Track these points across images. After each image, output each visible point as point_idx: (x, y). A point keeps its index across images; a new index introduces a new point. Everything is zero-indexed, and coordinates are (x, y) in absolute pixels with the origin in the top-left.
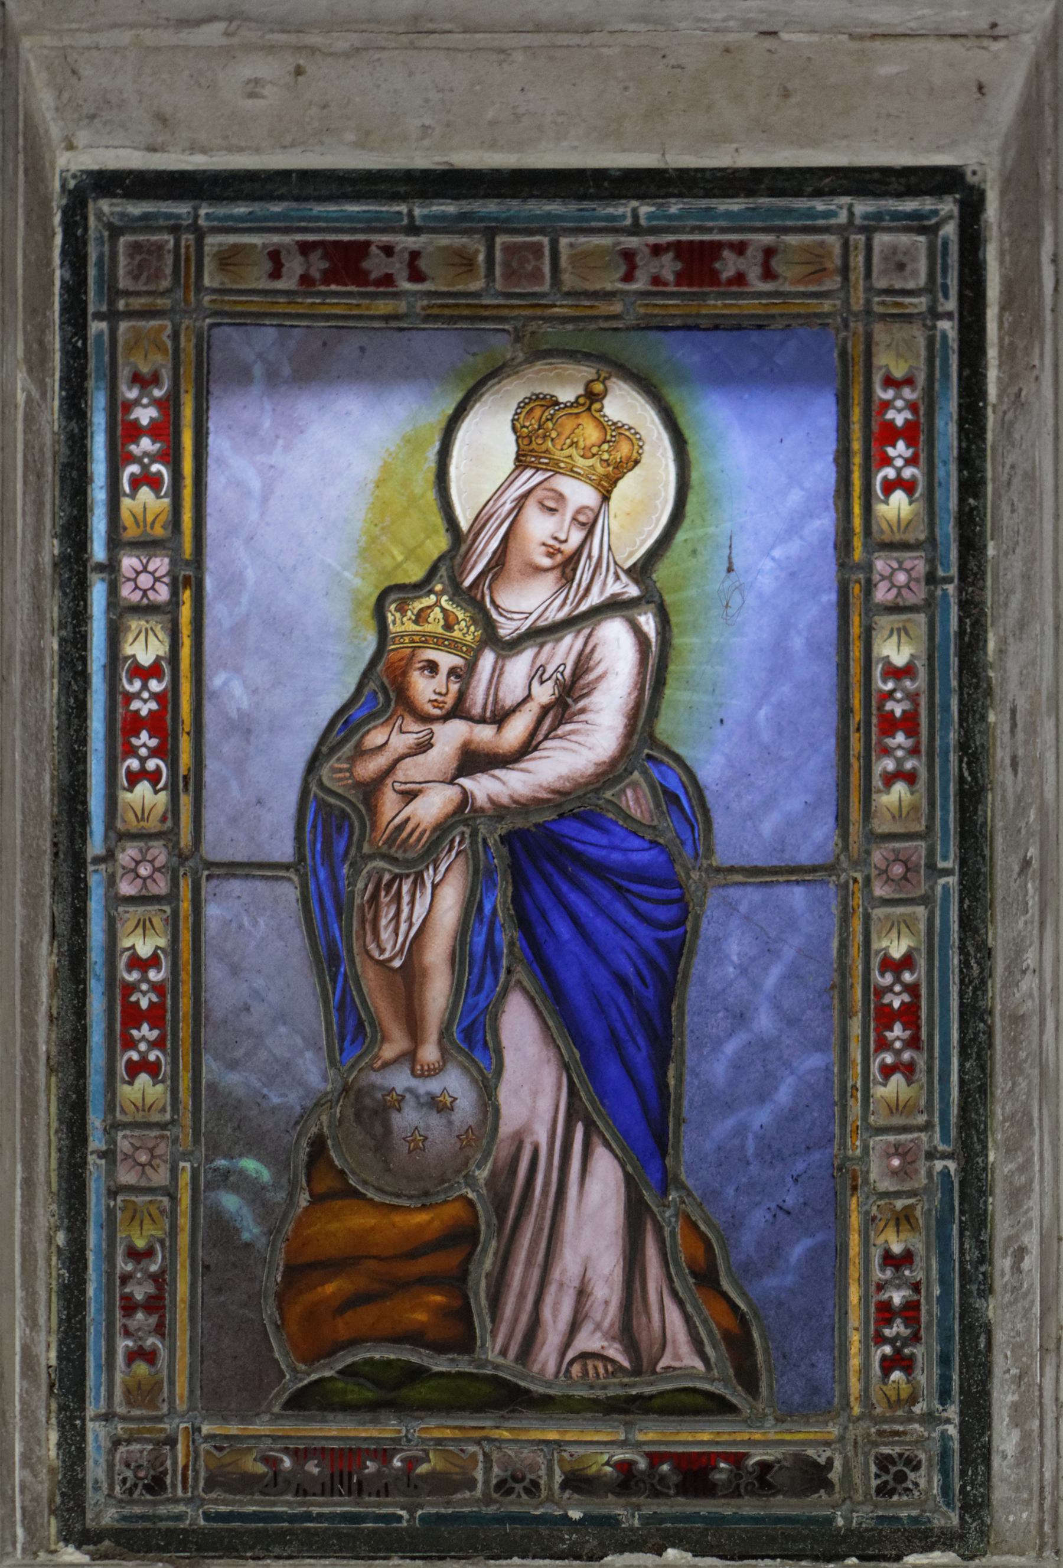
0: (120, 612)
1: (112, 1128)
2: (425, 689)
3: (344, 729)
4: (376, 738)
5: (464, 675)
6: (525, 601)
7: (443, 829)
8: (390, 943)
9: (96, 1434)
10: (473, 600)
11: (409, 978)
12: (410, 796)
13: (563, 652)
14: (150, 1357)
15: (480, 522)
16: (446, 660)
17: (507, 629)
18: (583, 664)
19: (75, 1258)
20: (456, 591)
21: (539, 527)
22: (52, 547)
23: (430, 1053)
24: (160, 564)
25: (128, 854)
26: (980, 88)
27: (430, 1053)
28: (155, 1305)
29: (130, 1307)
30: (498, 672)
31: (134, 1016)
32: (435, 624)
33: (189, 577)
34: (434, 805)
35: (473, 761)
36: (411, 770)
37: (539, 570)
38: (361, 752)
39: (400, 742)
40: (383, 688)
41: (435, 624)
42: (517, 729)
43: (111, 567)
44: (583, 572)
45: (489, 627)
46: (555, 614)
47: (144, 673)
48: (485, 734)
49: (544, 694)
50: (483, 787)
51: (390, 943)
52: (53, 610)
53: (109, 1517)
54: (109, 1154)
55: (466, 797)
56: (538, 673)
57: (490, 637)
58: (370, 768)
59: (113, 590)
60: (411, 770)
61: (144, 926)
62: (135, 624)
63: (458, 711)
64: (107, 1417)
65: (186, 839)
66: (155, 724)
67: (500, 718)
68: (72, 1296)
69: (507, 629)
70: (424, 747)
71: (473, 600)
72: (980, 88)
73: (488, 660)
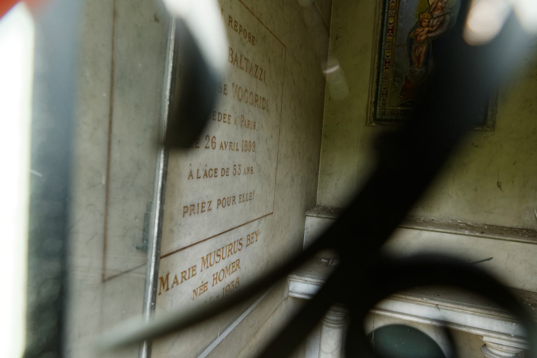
0: (388, 17)
1: (389, 9)
2: (424, 24)
3: (414, 28)
4: (418, 30)
5: (429, 22)
6: (437, 13)
7: (424, 40)
8: (417, 53)
9: (378, 108)
10: (431, 13)
11: (419, 58)
12: (421, 36)
13: (442, 18)
14: (385, 100)
15: (432, 4)
16: (427, 21)
17: (434, 16)
18: (444, 20)
19: (377, 90)
20: (429, 13)
21: (440, 4)
22: (381, 11)
23: (420, 66)
24: (394, 11)
25: (390, 11)
26: (514, 164)
27: (420, 66)
28: (386, 94)
29: (383, 94)
30: (433, 21)
31: (386, 62)
32: (426, 16)
33: (397, 14)
34: (423, 38)
35: (429, 32)
36: (421, 33)
37: (439, 9)
38: (415, 32)
39: (420, 30)
40: (419, 24)
41: (426, 16)
42: (434, 29)
43: (388, 12)
44: (444, 10)
45: (433, 16)
46: (441, 14)
47: (391, 24)
48: (430, 29)
49: (438, 24)
50: (430, 35)
51: (417, 53)
52: (381, 17)
53: (379, 117)
54: (388, 12)
55: (428, 36)
56: (438, 21)
57: (432, 17)
58: (417, 33)
59: (388, 15)
60: (421, 33)
61: (388, 52)
62: (390, 18)
63: (428, 26)
64: (380, 107)
65: (394, 42)
66: (392, 30)
67: (433, 27)
68: (377, 94)
69: (434, 16)
70: (423, 31)
71: (431, 13)
72: (514, 164)
73: (432, 20)
